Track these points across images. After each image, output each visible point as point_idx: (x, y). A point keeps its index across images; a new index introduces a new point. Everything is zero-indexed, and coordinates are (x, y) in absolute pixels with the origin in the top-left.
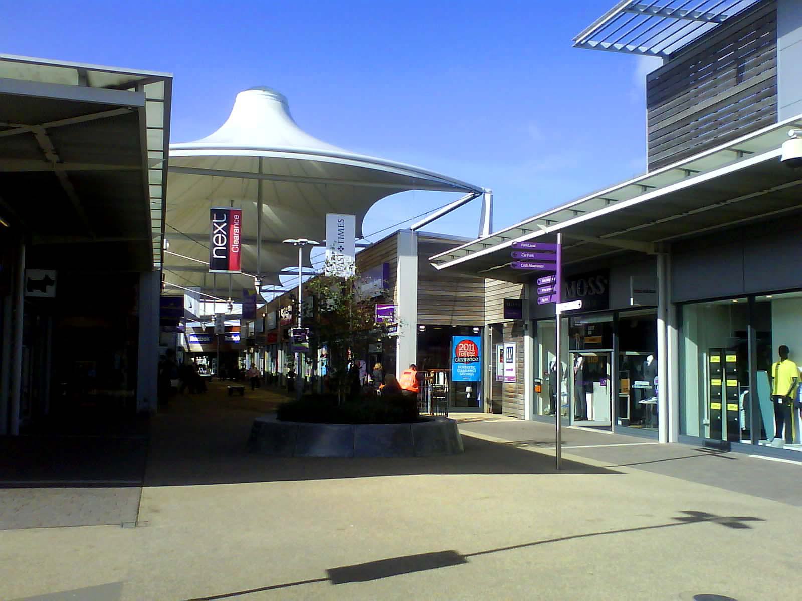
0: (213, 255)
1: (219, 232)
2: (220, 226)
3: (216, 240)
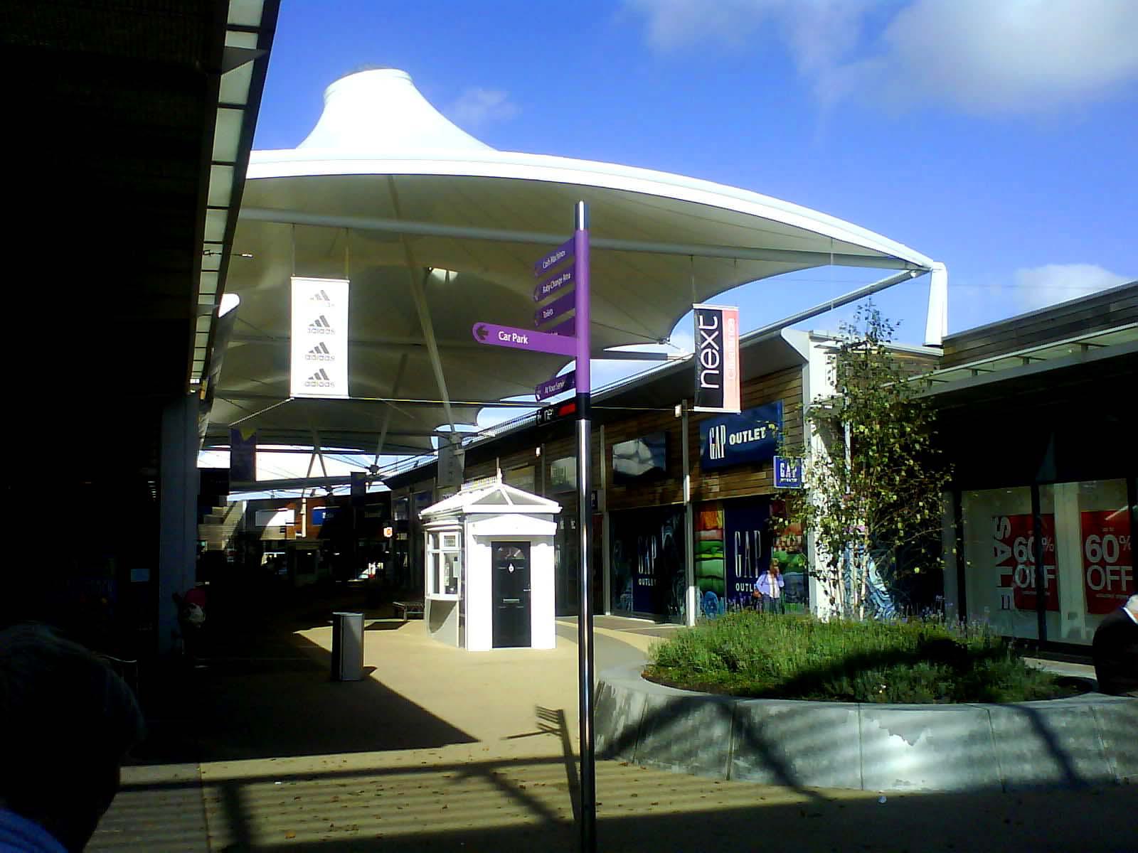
0: (701, 384)
1: (709, 346)
2: (710, 336)
3: (704, 357)
